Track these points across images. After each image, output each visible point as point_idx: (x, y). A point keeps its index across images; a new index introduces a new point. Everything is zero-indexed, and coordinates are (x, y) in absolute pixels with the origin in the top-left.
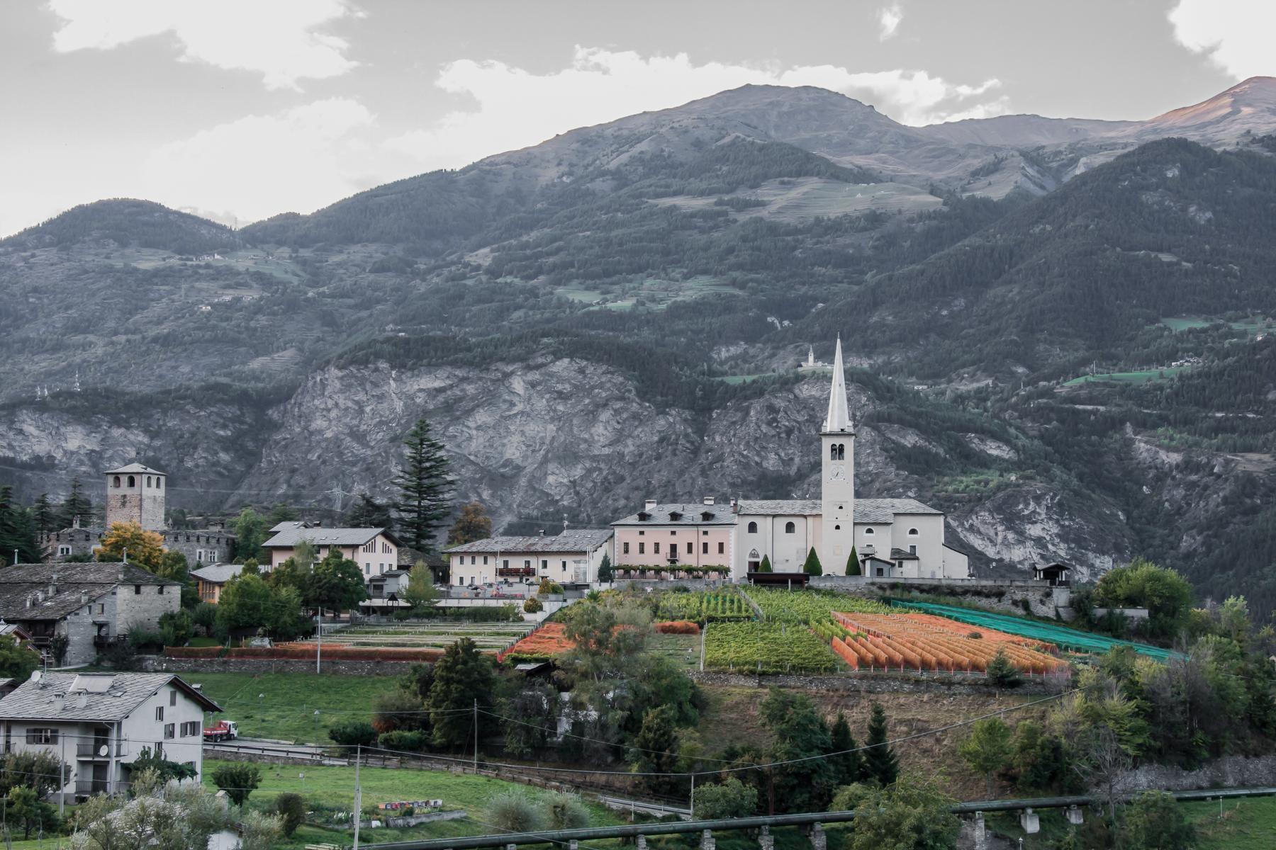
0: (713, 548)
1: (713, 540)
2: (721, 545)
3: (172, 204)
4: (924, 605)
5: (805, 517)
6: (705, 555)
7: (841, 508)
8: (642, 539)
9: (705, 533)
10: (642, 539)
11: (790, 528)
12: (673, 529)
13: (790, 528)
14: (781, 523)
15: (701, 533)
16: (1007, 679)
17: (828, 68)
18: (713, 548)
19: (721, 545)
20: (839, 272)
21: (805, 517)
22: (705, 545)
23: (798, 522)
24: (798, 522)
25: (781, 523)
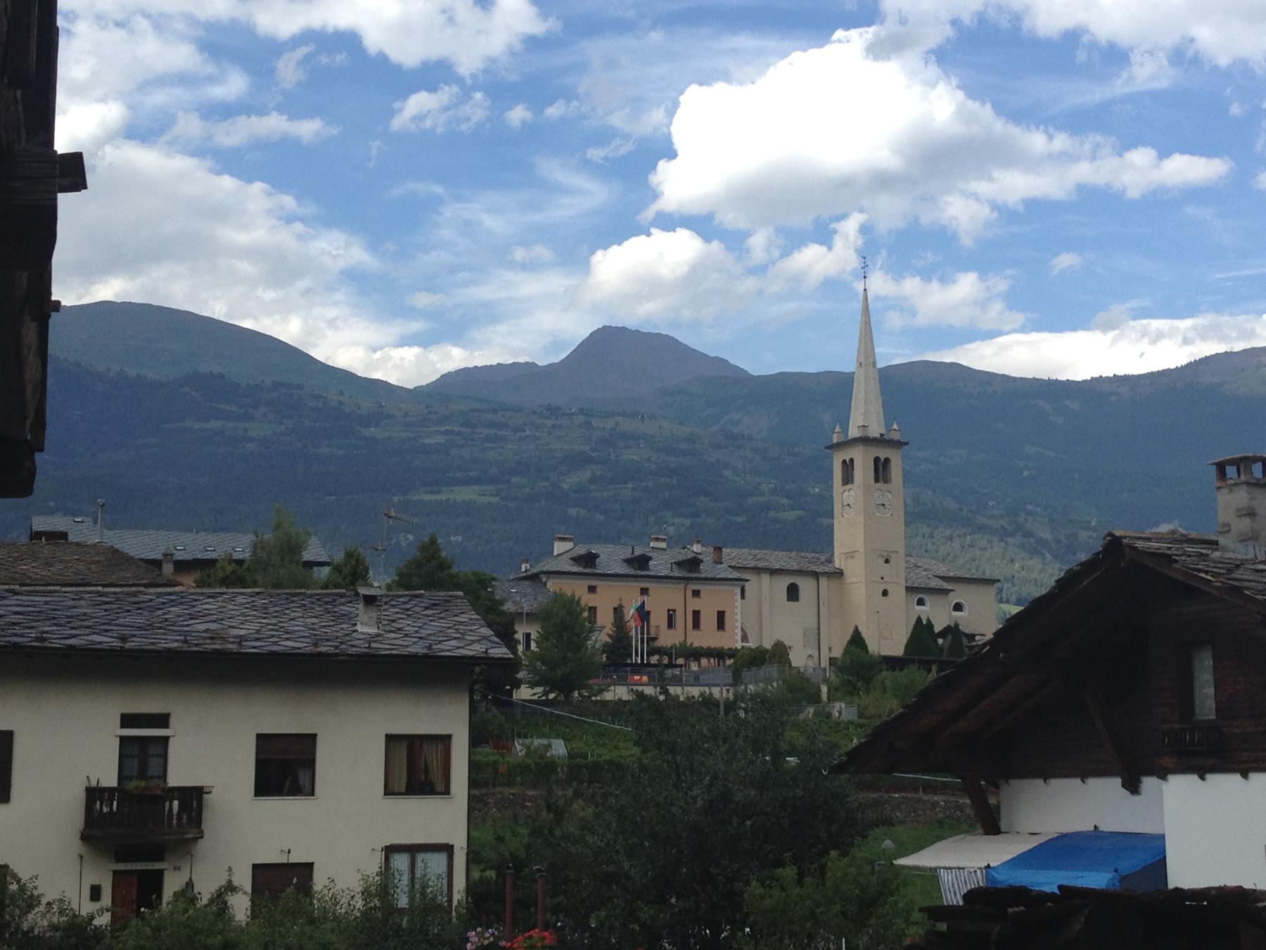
0: (709, 620)
1: (709, 603)
2: (721, 616)
3: (1155, 370)
4: (288, 648)
5: (816, 575)
6: (696, 633)
7: (887, 561)
8: (694, 604)
9: (696, 593)
10: (694, 604)
11: (793, 592)
12: (593, 583)
13: (793, 592)
14: (783, 583)
15: (689, 593)
16: (416, 326)
17: (1081, 371)
18: (709, 620)
19: (721, 616)
20: (96, 595)
21: (816, 575)
22: (696, 614)
23: (805, 585)
24: (805, 585)
25: (783, 583)
